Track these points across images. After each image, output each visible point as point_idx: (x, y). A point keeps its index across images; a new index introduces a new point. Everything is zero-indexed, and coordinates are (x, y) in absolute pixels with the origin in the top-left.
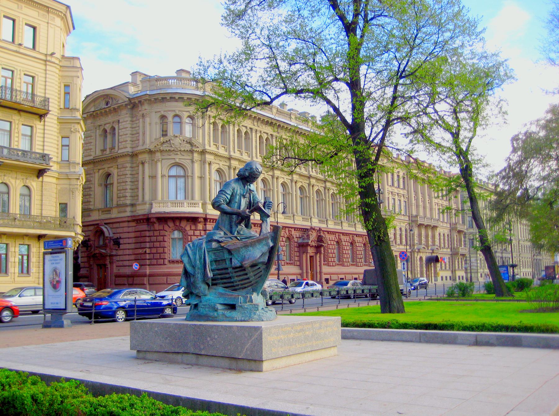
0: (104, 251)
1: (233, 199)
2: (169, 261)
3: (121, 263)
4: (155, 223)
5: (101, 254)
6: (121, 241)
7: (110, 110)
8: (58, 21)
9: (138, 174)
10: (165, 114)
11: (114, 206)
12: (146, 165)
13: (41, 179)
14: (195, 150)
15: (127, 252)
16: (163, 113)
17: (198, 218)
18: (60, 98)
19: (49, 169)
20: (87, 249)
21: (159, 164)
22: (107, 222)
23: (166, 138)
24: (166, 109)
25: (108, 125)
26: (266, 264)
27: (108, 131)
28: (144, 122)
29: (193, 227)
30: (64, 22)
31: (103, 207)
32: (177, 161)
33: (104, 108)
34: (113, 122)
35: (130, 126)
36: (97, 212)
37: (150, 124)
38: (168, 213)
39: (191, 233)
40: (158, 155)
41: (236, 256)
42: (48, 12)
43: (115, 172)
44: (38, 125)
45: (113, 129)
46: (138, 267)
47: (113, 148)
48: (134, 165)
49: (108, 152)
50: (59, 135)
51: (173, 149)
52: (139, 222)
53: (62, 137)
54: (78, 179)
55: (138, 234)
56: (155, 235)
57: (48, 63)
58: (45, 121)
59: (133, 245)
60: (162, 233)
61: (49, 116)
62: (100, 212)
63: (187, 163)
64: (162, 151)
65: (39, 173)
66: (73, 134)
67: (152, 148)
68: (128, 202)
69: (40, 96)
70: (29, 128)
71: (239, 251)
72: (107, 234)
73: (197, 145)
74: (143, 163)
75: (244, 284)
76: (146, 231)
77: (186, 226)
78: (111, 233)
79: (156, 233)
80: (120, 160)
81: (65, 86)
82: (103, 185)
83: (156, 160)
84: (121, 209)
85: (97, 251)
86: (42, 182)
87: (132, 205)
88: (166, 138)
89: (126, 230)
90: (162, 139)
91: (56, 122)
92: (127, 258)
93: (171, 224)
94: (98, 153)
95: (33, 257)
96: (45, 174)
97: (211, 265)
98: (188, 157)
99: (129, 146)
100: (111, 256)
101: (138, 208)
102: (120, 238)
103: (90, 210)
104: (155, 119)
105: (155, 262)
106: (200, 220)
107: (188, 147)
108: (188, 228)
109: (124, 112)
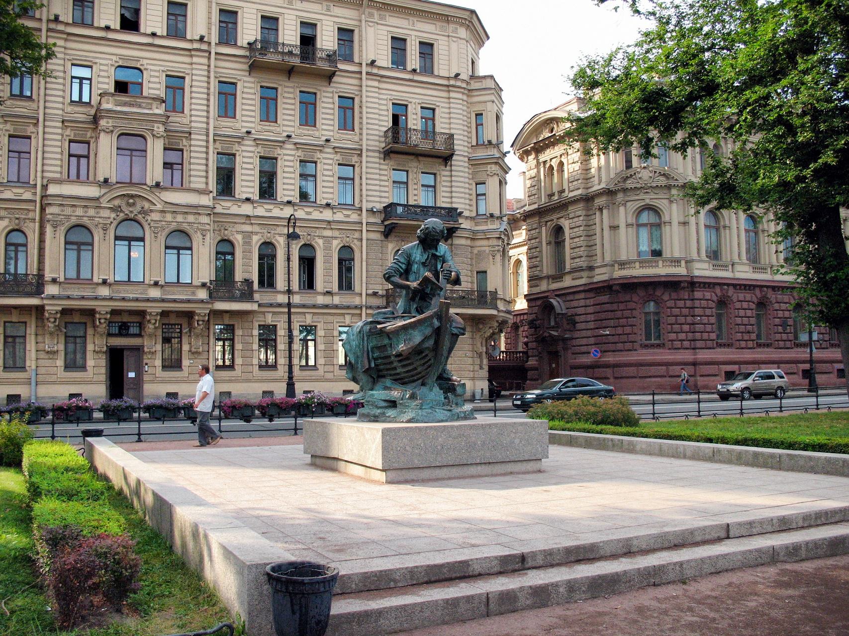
0: (556, 334)
3: (577, 349)
5: (551, 335)
8: (463, 32)
11: (567, 271)
12: (605, 211)
13: (449, 241)
15: (584, 334)
17: (680, 282)
21: (622, 209)
23: (631, 172)
27: (555, 169)
29: (674, 295)
30: (472, 32)
32: (648, 201)
39: (670, 303)
40: (620, 197)
42: (448, 22)
43: (566, 224)
44: (444, 172)
45: (561, 164)
48: (591, 212)
49: (556, 197)
53: (476, 184)
57: (451, 88)
58: (451, 166)
60: (631, 305)
61: (454, 158)
63: (662, 204)
64: (625, 190)
67: (612, 187)
68: (584, 265)
70: (432, 176)
72: (558, 310)
74: (601, 210)
75: (413, 376)
78: (563, 307)
79: (622, 306)
81: (476, 115)
82: (553, 242)
84: (577, 274)
85: (546, 334)
86: (452, 245)
88: (631, 172)
89: (582, 303)
91: (466, 165)
92: (584, 341)
93: (642, 293)
97: (373, 353)
100: (564, 340)
101: (597, 271)
102: (576, 315)
105: (743, 344)
106: (682, 285)
107: (662, 181)
108: (666, 297)
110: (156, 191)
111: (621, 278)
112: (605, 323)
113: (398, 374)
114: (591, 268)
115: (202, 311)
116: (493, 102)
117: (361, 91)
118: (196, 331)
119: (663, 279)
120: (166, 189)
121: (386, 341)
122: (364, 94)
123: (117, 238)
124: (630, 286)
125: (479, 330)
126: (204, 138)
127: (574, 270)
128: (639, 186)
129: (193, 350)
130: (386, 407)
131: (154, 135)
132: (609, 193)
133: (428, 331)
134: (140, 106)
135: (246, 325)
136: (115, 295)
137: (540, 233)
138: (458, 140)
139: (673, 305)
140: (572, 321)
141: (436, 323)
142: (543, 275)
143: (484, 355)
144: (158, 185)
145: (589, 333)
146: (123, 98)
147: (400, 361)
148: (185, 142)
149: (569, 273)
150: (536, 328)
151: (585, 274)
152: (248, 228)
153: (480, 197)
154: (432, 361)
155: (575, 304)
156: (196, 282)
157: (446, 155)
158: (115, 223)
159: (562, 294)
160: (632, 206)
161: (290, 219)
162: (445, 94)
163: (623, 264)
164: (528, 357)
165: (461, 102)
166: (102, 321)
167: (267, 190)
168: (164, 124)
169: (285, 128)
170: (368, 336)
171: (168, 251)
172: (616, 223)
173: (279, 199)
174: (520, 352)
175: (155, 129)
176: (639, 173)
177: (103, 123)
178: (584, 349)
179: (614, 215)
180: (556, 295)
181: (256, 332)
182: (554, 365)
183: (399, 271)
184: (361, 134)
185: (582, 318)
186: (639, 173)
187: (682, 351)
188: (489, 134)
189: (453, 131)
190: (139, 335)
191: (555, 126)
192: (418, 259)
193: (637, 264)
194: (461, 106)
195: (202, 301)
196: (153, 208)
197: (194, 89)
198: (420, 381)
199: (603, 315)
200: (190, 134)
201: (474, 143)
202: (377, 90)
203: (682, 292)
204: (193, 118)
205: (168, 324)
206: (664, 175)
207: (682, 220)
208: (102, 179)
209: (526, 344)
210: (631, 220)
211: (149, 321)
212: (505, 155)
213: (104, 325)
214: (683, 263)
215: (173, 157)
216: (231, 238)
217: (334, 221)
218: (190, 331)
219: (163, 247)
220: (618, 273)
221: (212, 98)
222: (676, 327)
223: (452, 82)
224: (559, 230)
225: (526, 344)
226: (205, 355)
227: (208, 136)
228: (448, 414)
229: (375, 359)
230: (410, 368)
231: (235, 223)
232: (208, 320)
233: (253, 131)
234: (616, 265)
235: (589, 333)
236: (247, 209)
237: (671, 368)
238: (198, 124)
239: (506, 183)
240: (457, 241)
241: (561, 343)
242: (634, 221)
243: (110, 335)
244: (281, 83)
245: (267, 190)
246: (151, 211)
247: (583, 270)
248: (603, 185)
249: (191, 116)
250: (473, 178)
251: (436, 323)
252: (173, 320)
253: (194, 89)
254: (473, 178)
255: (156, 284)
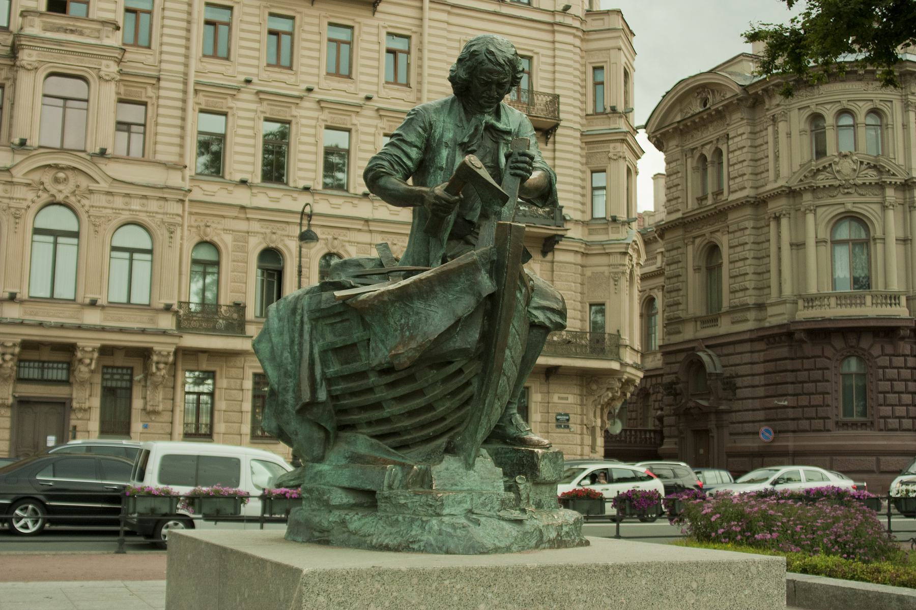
1: (433, 160)
2: (837, 423)
3: (738, 428)
4: (805, 342)
5: (699, 407)
6: (739, 382)
7: (710, 115)
9: (769, 241)
10: (820, 110)
11: (723, 310)
12: (784, 222)
13: (549, 257)
14: (888, 181)
15: (749, 404)
16: (814, 109)
18: (584, 95)
19: (562, 236)
20: (675, 399)
21: (810, 217)
22: (710, 343)
23: (824, 162)
24: (821, 100)
25: (708, 147)
26: (480, 357)
27: (709, 159)
28: (776, 133)
29: (889, 349)
31: (704, 314)
32: (849, 207)
33: (700, 113)
34: (718, 139)
35: (749, 143)
36: (693, 323)
37: (789, 135)
38: (829, 320)
39: (884, 361)
40: (807, 198)
41: (378, 329)
43: (724, 241)
45: (719, 152)
46: (771, 436)
47: (720, 192)
48: (762, 223)
49: (710, 201)
50: (584, 168)
51: (838, 183)
52: (771, 339)
53: (592, 172)
54: (625, 253)
55: (771, 366)
56: (806, 367)
57: (556, 28)
58: (554, 143)
59: (762, 389)
60: (821, 362)
61: (559, 131)
62: (699, 323)
64: (814, 190)
65: (544, 245)
66: (613, 163)
67: (794, 184)
68: (751, 301)
69: (545, 94)
71: (385, 315)
72: (710, 368)
73: (892, 171)
74: (777, 219)
76: (785, 359)
77: (872, 345)
79: (808, 364)
80: (732, 217)
81: (595, 68)
83: (802, 209)
84: (739, 316)
85: (691, 404)
86: (553, 262)
87: (761, 307)
88: (824, 162)
89: (747, 358)
90: (814, 165)
91: (578, 142)
92: (749, 416)
93: (839, 343)
94: (692, 204)
95: (536, 412)
96: (556, 246)
97: (324, 363)
98: (872, 197)
99: (748, 184)
100: (719, 413)
101: (771, 311)
102: (738, 376)
103: (680, 321)
104: (798, 121)
105: (804, 424)
106: (902, 333)
107: (872, 176)
108: (876, 351)
109: (737, 116)
110: (102, 163)
111: (808, 321)
112: (781, 389)
113: (387, 420)
114: (761, 307)
115: (164, 347)
116: (620, 49)
117: (421, 26)
118: (155, 379)
119: (872, 324)
120: (116, 158)
121: (357, 334)
122: (427, 31)
123: (37, 231)
124: (822, 333)
125: (591, 393)
126: (181, 86)
127: (734, 310)
128: (837, 183)
129: (149, 408)
130: (351, 507)
131: (100, 78)
132: (792, 193)
133: (464, 304)
134: (81, 34)
135: (234, 372)
136: (28, 318)
137: (685, 254)
138: (565, 104)
139: (887, 363)
140: (730, 384)
141: (487, 284)
142: (689, 316)
143: (598, 430)
144: (103, 153)
145: (757, 404)
146: (58, 20)
147: (392, 385)
148: (150, 91)
149: (728, 313)
150: (676, 395)
151: (751, 315)
152: (242, 225)
153: (596, 193)
154: (474, 388)
155: (736, 359)
156: (160, 303)
157: (547, 127)
158: (34, 208)
159: (716, 345)
160: (826, 214)
161: (303, 213)
162: (548, 37)
163: (810, 300)
164: (662, 438)
165: (571, 48)
166: (8, 357)
167: (275, 169)
168: (119, 62)
169: (304, 78)
170: (315, 320)
171: (115, 254)
172: (800, 239)
173: (292, 184)
174: (650, 431)
175: (103, 68)
176: (836, 163)
177: (26, 57)
178: (748, 427)
179: (799, 225)
180: (707, 347)
181: (249, 384)
182: (702, 451)
183: (401, 163)
184: (419, 91)
185: (748, 381)
186: (836, 163)
187: (899, 433)
188: (613, 97)
189: (557, 92)
190: (67, 382)
191: (710, 97)
192: (449, 136)
193: (833, 301)
194: (571, 55)
195: (164, 333)
196: (93, 186)
197: (167, 13)
198: (442, 441)
199: (778, 378)
200: (159, 79)
201: (590, 111)
202: (445, 26)
203: (901, 343)
204: (165, 57)
205: (113, 367)
206: (875, 167)
207: (901, 235)
208: (17, 141)
209: (660, 419)
210: (824, 234)
211: (81, 361)
212: (635, 131)
213: (10, 364)
214: (903, 300)
215: (132, 114)
216: (216, 239)
217: (374, 220)
218: (145, 379)
219: (108, 248)
220: (804, 314)
221: (194, 28)
222: (892, 398)
223: (559, 18)
224: (713, 250)
225: (660, 419)
226: (166, 417)
227: (185, 83)
228: (512, 530)
229: (330, 381)
230: (419, 402)
231: (223, 217)
232: (174, 364)
233: (255, 80)
234: (800, 302)
235: (757, 404)
236: (241, 197)
237: (883, 459)
238: (172, 67)
239: (637, 173)
240: (559, 257)
241: (713, 417)
242: (828, 238)
243: (20, 380)
244: (299, 9)
245: (275, 169)
246: (91, 192)
247: (749, 309)
248: (781, 183)
249: (161, 53)
250: (587, 164)
251: (487, 284)
252: (119, 360)
253: (167, 13)
254: (587, 164)
255: (93, 304)
